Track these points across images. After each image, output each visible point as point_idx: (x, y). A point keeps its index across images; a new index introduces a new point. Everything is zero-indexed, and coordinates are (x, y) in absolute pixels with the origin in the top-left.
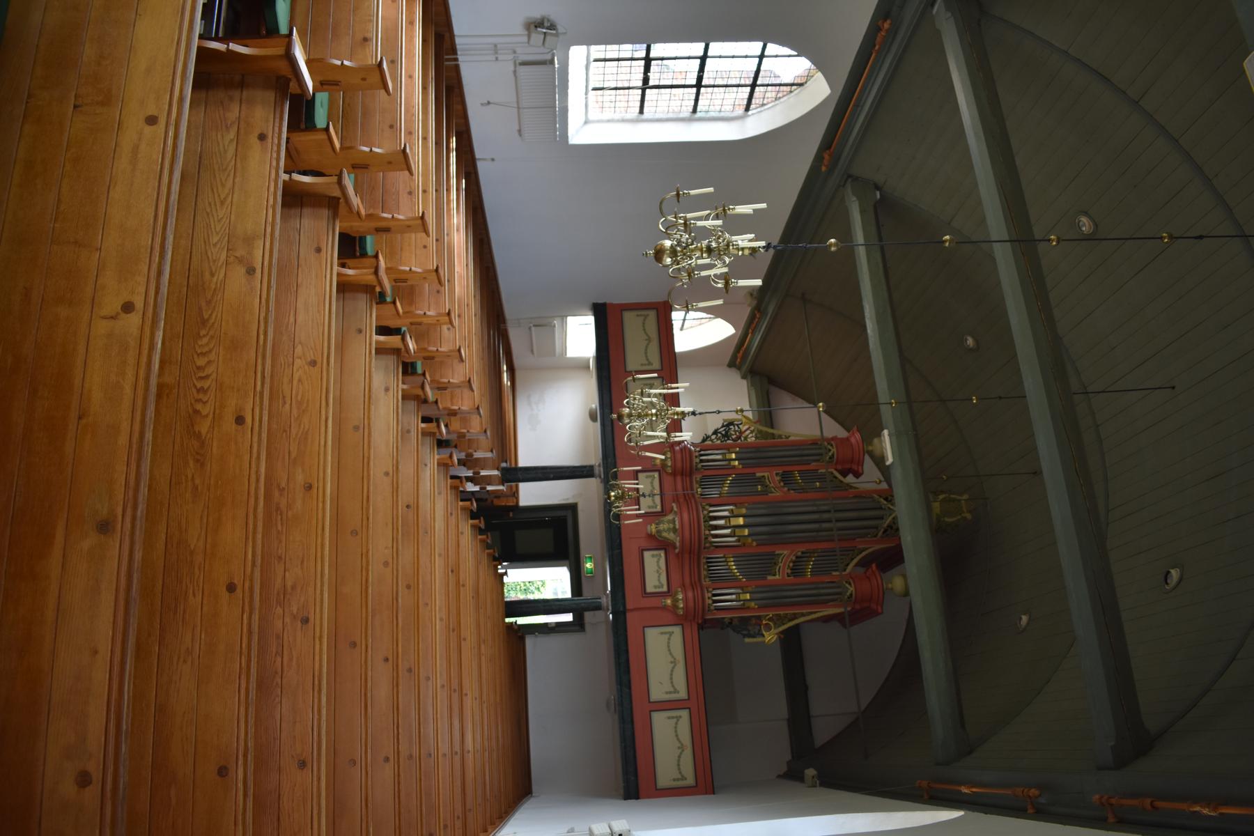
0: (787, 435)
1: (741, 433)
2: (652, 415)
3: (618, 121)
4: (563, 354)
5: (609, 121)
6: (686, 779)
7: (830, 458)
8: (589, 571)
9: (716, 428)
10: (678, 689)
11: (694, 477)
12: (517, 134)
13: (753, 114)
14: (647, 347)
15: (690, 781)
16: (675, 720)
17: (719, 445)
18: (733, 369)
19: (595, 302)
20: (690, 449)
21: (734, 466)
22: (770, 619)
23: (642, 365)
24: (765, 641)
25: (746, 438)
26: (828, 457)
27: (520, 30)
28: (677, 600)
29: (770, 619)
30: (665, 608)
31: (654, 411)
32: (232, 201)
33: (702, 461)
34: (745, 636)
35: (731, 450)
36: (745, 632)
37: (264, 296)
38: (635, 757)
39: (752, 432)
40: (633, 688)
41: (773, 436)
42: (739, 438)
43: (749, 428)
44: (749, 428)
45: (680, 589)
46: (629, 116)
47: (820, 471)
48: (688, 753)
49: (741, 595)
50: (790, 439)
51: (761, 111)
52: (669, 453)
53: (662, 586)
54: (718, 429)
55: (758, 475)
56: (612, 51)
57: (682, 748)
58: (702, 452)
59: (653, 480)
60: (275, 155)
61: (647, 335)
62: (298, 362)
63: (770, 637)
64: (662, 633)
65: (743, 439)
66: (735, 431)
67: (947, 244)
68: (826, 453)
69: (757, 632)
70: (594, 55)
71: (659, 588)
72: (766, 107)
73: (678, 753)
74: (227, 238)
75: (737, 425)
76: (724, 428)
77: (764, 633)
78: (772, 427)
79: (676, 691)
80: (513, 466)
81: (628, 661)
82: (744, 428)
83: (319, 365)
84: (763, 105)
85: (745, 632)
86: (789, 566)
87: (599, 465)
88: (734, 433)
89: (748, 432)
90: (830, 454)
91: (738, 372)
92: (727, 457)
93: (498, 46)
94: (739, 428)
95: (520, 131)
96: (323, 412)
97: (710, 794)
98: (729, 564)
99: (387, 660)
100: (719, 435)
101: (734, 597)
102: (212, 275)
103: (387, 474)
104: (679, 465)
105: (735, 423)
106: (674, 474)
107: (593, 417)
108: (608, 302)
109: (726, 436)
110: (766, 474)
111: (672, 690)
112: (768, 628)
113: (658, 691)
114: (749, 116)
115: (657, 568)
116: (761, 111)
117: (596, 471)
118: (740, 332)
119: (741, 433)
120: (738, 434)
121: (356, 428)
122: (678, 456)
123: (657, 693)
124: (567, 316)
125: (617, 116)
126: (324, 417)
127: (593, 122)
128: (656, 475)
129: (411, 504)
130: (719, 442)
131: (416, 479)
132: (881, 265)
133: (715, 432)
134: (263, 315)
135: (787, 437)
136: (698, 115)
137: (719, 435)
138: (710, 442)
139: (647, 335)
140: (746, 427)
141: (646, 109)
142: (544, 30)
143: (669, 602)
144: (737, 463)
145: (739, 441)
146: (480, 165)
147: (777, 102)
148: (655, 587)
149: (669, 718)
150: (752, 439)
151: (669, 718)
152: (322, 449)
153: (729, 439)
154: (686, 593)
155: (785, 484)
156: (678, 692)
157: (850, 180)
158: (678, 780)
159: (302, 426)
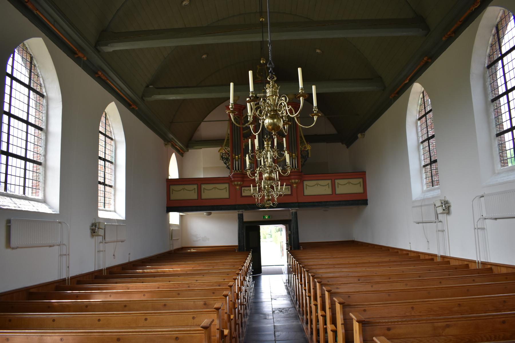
0: (228, 134)
1: (226, 153)
2: (268, 187)
3: (115, 197)
4: (178, 226)
5: (115, 202)
6: (360, 182)
7: (238, 118)
8: (269, 217)
9: (224, 163)
10: (225, 187)
11: (244, 173)
12: (123, 243)
13: (114, 137)
14: (187, 190)
15: (361, 180)
16: (339, 185)
17: (231, 163)
18: (184, 155)
19: (166, 211)
20: (233, 174)
21: (241, 156)
22: (302, 146)
23: (195, 192)
24: (310, 149)
25: (228, 151)
26: (239, 119)
27: (93, 240)
28: (295, 182)
29: (302, 146)
30: (297, 187)
31: (266, 186)
32: (420, 337)
33: (238, 170)
34: (308, 157)
35: (234, 157)
36: (307, 157)
37: (457, 320)
38: (353, 201)
39: (226, 149)
40: (293, 202)
41: (228, 140)
42: (228, 154)
43: (224, 149)
44: (224, 149)
45: (290, 181)
46: (113, 192)
47: (243, 123)
48: (352, 181)
49: (293, 157)
50: (229, 133)
51: (114, 133)
52: (235, 183)
53: (288, 188)
54: (224, 162)
55: (244, 147)
56: (101, 199)
57: (349, 183)
58: (234, 169)
59: (245, 190)
60: (396, 323)
61: (182, 190)
62: (413, 314)
63: (309, 147)
64: (306, 189)
65: (228, 153)
66: (225, 155)
67: (264, 62)
68: (237, 119)
69: (306, 152)
70: (103, 208)
71: (289, 189)
72: (112, 131)
73: (319, 186)
74: (435, 337)
75: (222, 154)
76: (224, 160)
77: (307, 149)
78: (224, 140)
79: (328, 184)
80: (238, 247)
81: (283, 203)
82: (224, 152)
83: (413, 306)
84: (111, 132)
85: (307, 157)
86: (281, 138)
87: (238, 211)
88: (226, 156)
89: (226, 150)
90: (237, 118)
91: (185, 153)
92: (237, 159)
93: (98, 250)
94: (224, 154)
95: (122, 242)
96: (431, 302)
97: (366, 173)
98: (280, 161)
99: (440, 282)
100: (227, 162)
101: (294, 160)
102: (451, 340)
103: (372, 286)
104: (239, 179)
105: (222, 155)
106: (243, 181)
107: (210, 214)
108: (166, 206)
109: (227, 159)
110: (244, 144)
111: (328, 186)
112: (305, 148)
113: (328, 191)
114: (115, 138)
115: (249, 191)
116: (114, 133)
117: (240, 213)
118: (175, 152)
119: (226, 153)
120: (226, 154)
121: (389, 295)
122: (236, 179)
123: (329, 191)
124: (169, 224)
125: (112, 197)
126: (433, 302)
127: (115, 208)
128: (243, 188)
129: (357, 279)
130: (230, 162)
131: (348, 278)
132: (185, 89)
133: (226, 164)
134: (464, 319)
135: (229, 135)
136: (113, 161)
137: (227, 162)
138: (230, 166)
139: (182, 190)
140: (224, 151)
141: (111, 184)
142: (97, 229)
143: (295, 185)
144: (239, 155)
145: (230, 154)
146: (132, 259)
147: (111, 126)
148: (289, 190)
149: (338, 187)
150: (229, 149)
151: (338, 187)
152: (445, 302)
153: (229, 158)
154: (292, 179)
155: (248, 137)
156: (329, 183)
157: (144, 98)
158: (360, 185)
159: (437, 310)
